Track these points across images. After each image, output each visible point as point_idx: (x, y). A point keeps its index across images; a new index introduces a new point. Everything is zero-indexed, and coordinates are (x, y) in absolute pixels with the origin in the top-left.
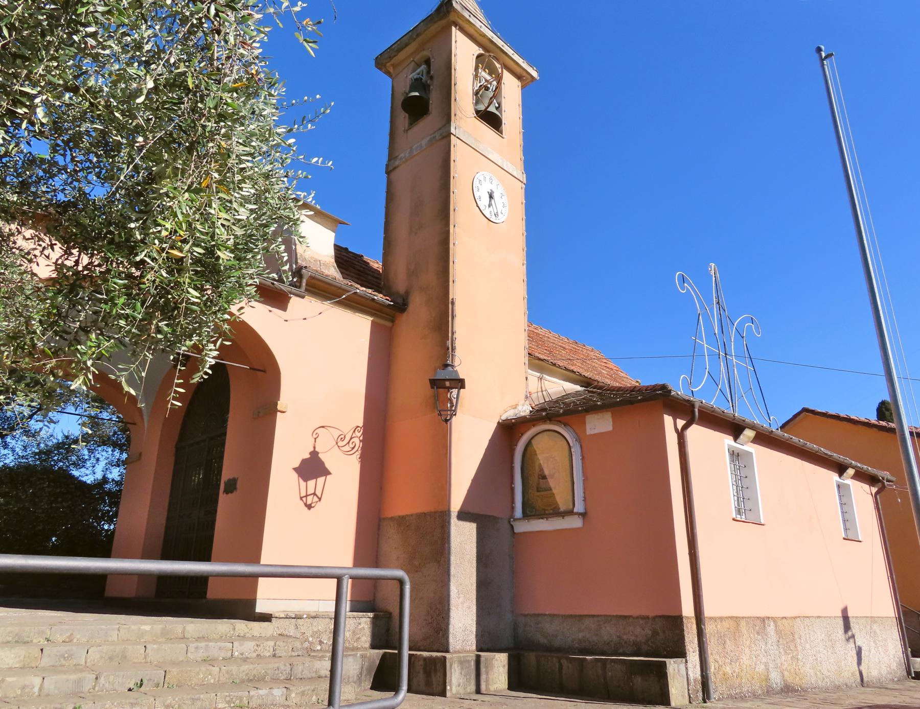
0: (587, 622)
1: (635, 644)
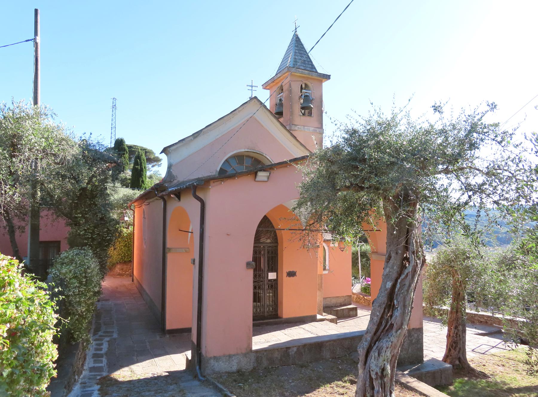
1: (340, 303)
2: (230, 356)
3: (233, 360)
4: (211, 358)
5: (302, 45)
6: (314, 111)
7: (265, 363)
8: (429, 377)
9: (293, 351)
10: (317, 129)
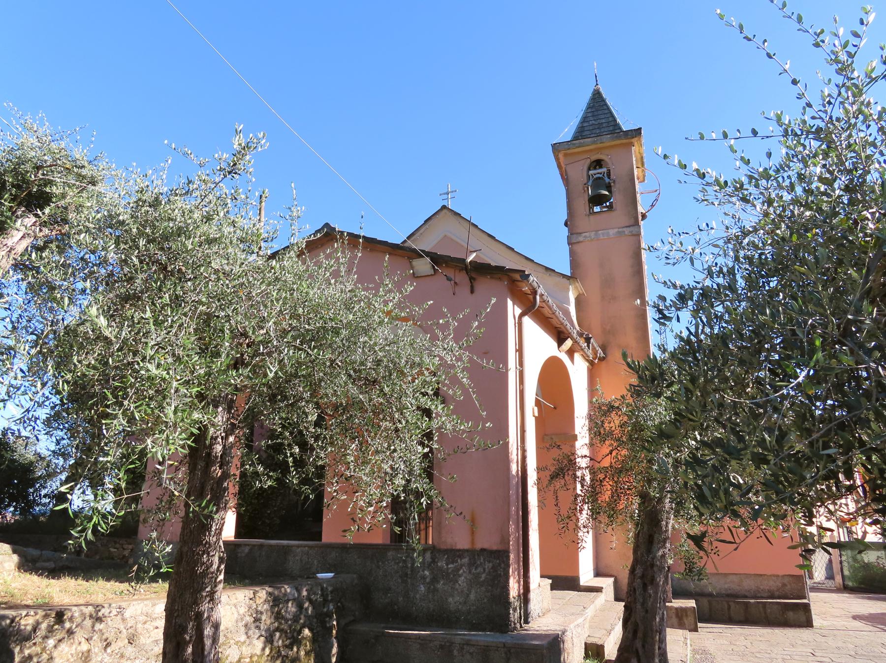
0: (731, 578)
1: (769, 591)
8: (471, 654)
10: (625, 229)
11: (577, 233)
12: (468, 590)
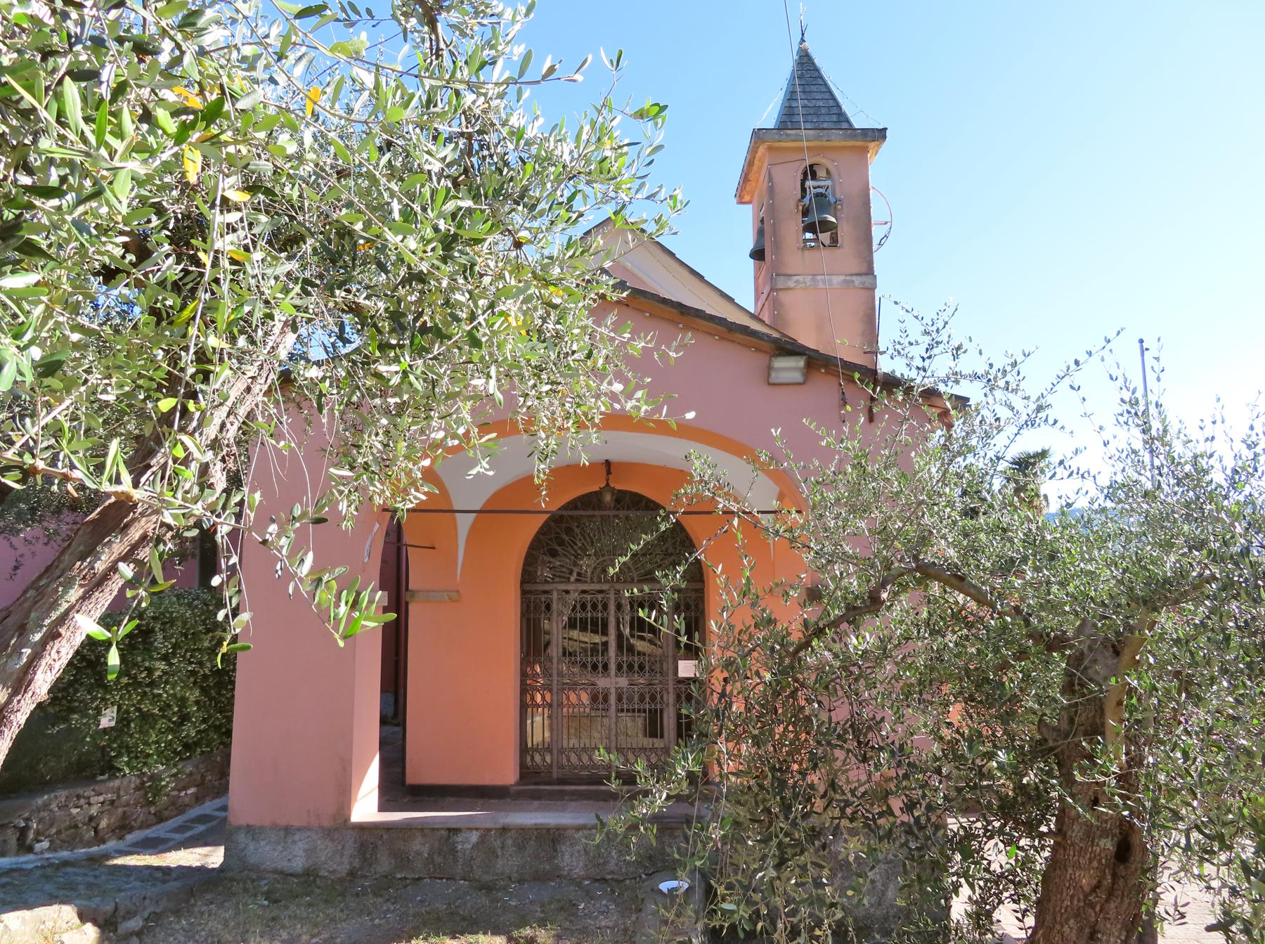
2: (288, 830)
3: (294, 842)
4: (239, 828)
5: (817, 70)
6: (845, 233)
7: (384, 864)
9: (467, 840)
10: (854, 278)
11: (784, 275)
12: (883, 885)
